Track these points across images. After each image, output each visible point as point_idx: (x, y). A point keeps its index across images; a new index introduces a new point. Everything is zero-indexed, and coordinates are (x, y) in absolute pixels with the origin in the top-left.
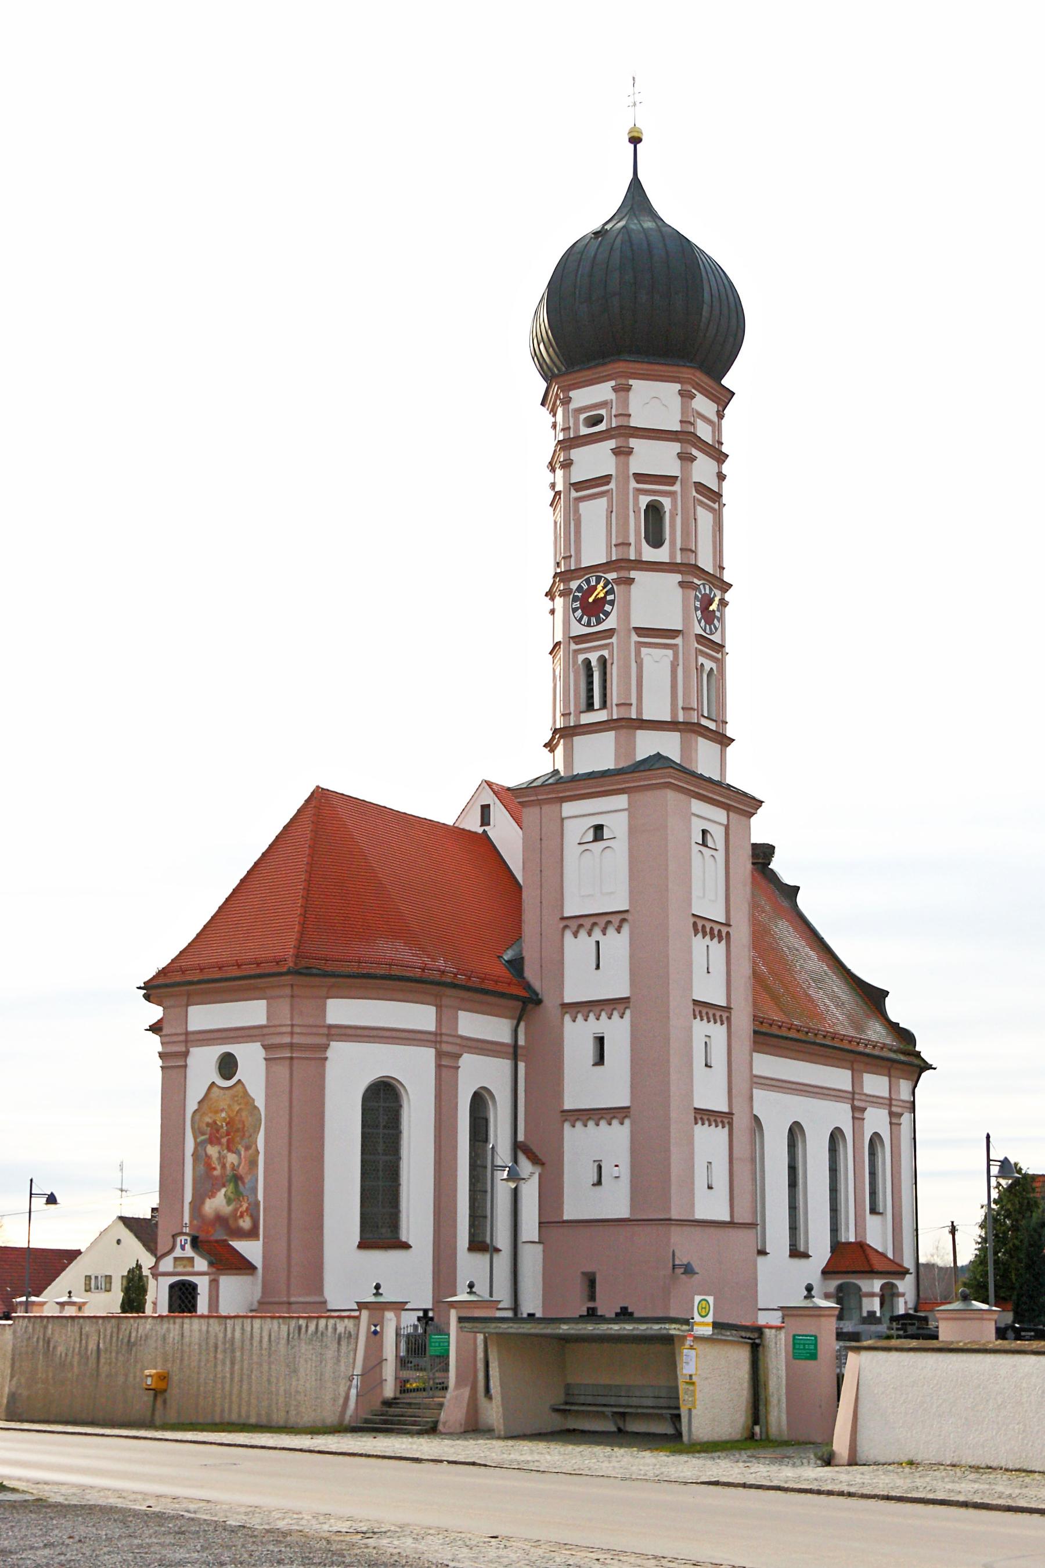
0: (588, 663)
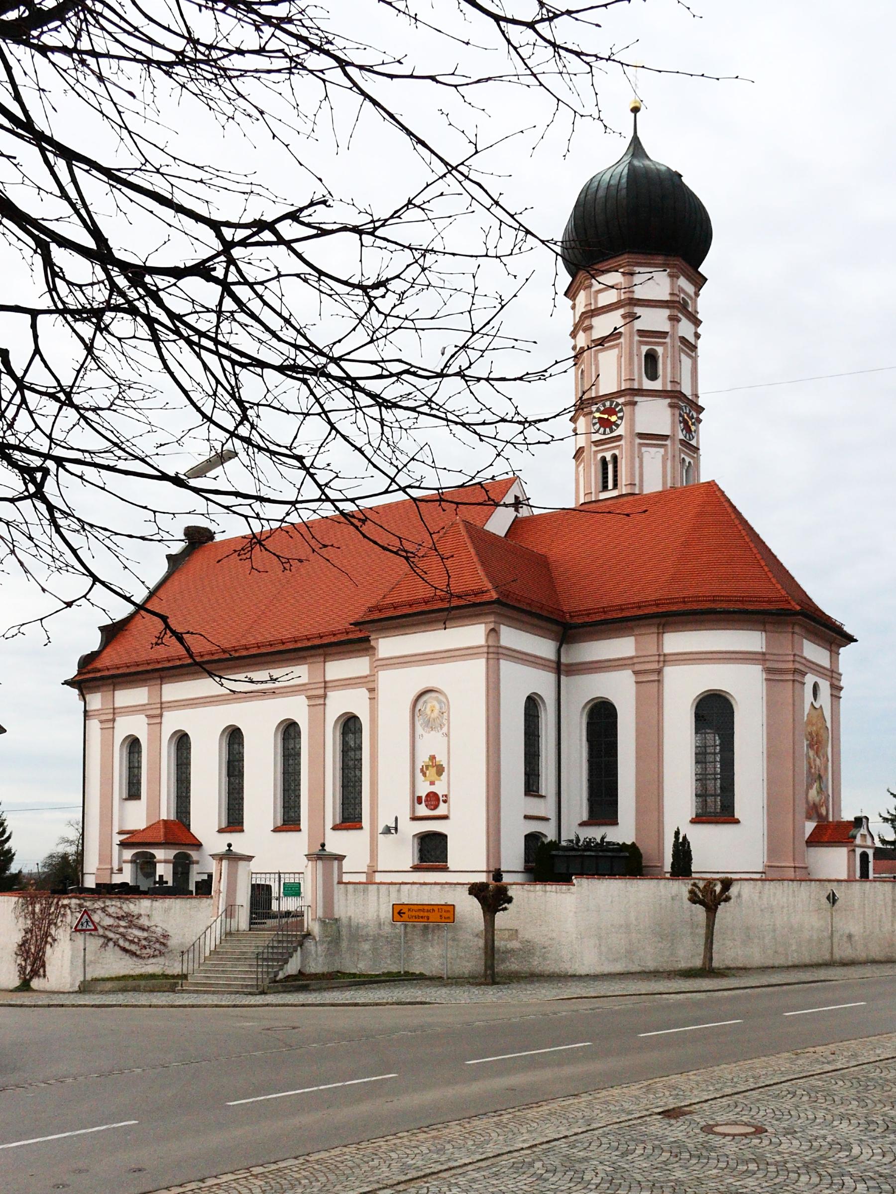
0: (604, 459)
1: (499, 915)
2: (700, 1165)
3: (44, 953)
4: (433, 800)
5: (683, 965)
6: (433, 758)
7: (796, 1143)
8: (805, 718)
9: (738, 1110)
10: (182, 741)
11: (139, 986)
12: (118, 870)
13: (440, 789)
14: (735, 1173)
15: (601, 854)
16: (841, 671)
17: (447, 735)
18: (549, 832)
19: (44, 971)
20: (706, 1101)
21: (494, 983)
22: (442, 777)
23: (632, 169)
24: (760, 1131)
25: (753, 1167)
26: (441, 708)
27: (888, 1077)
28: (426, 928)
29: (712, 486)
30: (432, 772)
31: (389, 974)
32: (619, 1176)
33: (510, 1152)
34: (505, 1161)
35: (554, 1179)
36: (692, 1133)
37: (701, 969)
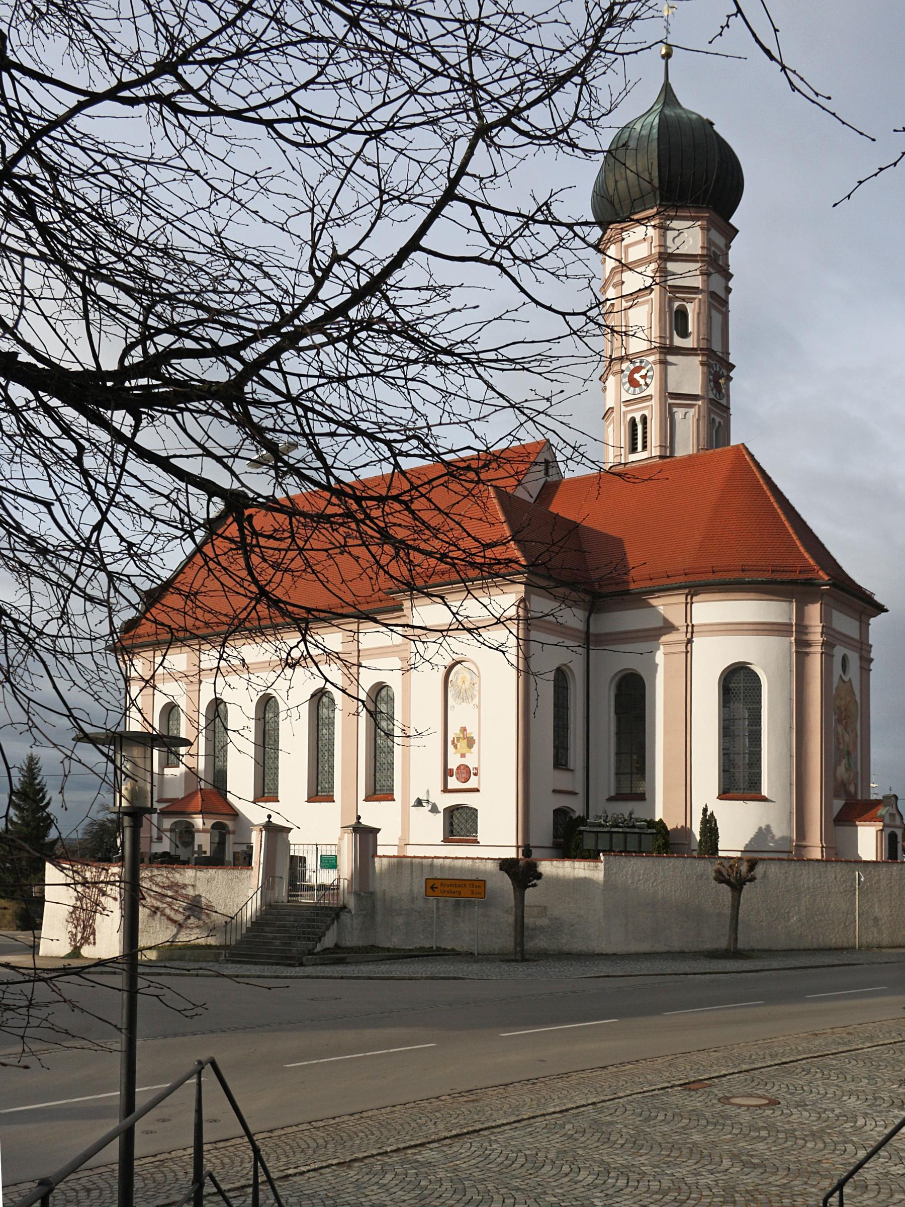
0: (633, 420)
1: (529, 892)
2: (716, 1131)
3: (94, 920)
4: (465, 773)
5: (708, 946)
6: (464, 730)
7: (806, 1114)
8: (834, 692)
9: (754, 1084)
10: (217, 707)
11: (185, 955)
12: (157, 839)
13: (470, 761)
14: (747, 1139)
15: (628, 830)
16: (871, 642)
17: (479, 707)
18: (577, 807)
19: (94, 939)
20: (725, 1076)
21: (524, 960)
22: (472, 750)
23: (664, 122)
24: (773, 1103)
25: (764, 1133)
26: (472, 679)
27: (901, 1058)
28: (457, 903)
29: (743, 449)
30: (463, 744)
31: (422, 949)
32: (642, 1137)
33: (544, 1115)
34: (539, 1122)
35: (583, 1139)
36: (710, 1104)
37: (726, 950)
